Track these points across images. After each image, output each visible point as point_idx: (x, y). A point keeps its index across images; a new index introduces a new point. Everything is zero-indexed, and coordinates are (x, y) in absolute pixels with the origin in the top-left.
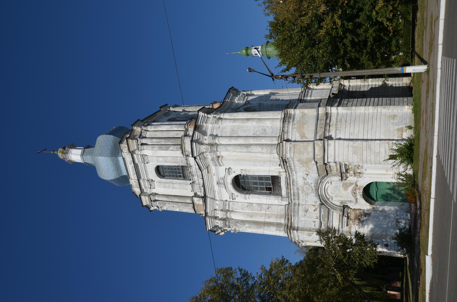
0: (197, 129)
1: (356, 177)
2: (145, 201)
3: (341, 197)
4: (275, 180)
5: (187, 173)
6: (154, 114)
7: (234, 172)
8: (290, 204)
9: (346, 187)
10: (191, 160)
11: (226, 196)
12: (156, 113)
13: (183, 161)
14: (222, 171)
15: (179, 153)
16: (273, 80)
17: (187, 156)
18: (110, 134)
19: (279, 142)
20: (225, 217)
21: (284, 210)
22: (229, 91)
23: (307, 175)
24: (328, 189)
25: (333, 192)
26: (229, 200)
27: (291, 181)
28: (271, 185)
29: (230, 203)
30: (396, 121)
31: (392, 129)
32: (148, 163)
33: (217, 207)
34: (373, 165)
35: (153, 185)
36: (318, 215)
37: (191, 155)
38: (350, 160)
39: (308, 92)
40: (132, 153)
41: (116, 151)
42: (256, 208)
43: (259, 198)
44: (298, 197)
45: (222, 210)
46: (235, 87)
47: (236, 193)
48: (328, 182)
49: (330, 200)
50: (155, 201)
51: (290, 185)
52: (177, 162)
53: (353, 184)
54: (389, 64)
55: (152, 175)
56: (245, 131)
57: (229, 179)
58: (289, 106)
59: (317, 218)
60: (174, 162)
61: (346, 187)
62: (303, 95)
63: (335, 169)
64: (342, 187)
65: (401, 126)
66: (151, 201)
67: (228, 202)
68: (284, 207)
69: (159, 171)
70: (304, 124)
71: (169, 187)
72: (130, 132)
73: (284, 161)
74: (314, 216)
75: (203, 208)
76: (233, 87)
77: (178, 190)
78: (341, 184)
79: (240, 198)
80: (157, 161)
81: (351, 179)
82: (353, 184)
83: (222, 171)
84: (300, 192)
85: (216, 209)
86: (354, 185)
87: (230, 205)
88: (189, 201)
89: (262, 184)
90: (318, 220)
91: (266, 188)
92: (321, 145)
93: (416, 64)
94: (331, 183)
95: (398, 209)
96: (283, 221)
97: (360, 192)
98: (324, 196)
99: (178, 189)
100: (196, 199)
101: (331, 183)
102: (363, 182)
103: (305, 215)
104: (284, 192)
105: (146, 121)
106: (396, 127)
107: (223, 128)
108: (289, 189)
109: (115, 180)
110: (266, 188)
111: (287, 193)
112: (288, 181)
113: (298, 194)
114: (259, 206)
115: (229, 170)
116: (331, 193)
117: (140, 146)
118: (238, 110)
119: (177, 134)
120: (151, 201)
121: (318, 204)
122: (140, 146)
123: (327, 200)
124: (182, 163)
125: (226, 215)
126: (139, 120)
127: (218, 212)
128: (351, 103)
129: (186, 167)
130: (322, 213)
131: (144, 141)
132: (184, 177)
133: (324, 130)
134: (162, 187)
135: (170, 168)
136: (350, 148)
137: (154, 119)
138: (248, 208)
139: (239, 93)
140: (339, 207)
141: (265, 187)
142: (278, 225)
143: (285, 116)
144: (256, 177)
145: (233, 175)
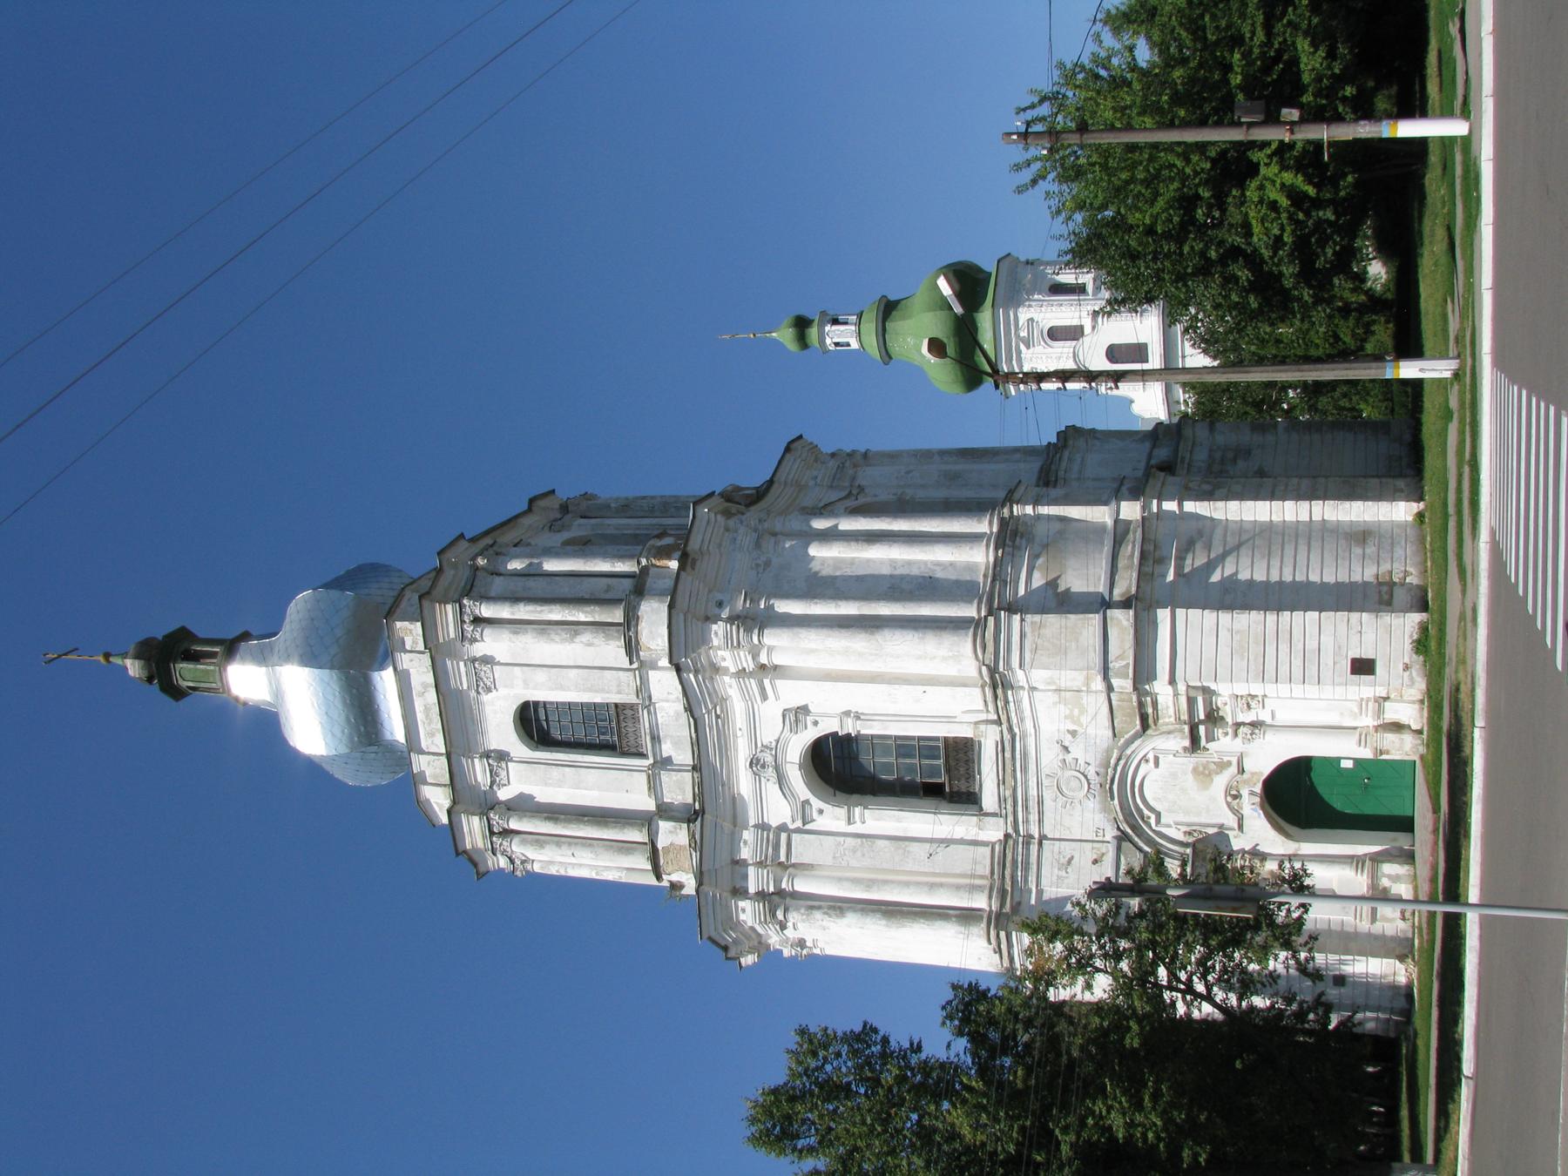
0: (689, 568)
1: (1239, 740)
4: (961, 753)
6: (509, 521)
8: (1011, 842)
9: (1204, 775)
11: (778, 811)
20: (772, 889)
23: (1073, 733)
32: (489, 690)
35: (503, 774)
37: (664, 662)
40: (436, 651)
44: (1041, 813)
47: (816, 803)
48: (1145, 759)
49: (1153, 821)
50: (507, 833)
52: (603, 691)
53: (1229, 763)
55: (499, 729)
57: (797, 745)
58: (1017, 496)
60: (590, 690)
61: (1204, 775)
63: (1171, 712)
66: (492, 833)
68: (988, 850)
69: (535, 724)
73: (998, 683)
76: (800, 437)
79: (831, 816)
80: (526, 683)
81: (1223, 745)
82: (1229, 763)
84: (1048, 796)
86: (1234, 769)
92: (1125, 623)
93: (1326, 674)
94: (1157, 764)
95: (1394, 90)
96: (980, 902)
100: (664, 826)
101: (1157, 764)
102: (1266, 756)
104: (989, 800)
109: (332, 759)
111: (1001, 800)
113: (1040, 802)
117: (469, 628)
119: (609, 588)
121: (1108, 837)
125: (777, 882)
126: (462, 536)
129: (632, 707)
134: (534, 777)
138: (859, 854)
145: (810, 735)
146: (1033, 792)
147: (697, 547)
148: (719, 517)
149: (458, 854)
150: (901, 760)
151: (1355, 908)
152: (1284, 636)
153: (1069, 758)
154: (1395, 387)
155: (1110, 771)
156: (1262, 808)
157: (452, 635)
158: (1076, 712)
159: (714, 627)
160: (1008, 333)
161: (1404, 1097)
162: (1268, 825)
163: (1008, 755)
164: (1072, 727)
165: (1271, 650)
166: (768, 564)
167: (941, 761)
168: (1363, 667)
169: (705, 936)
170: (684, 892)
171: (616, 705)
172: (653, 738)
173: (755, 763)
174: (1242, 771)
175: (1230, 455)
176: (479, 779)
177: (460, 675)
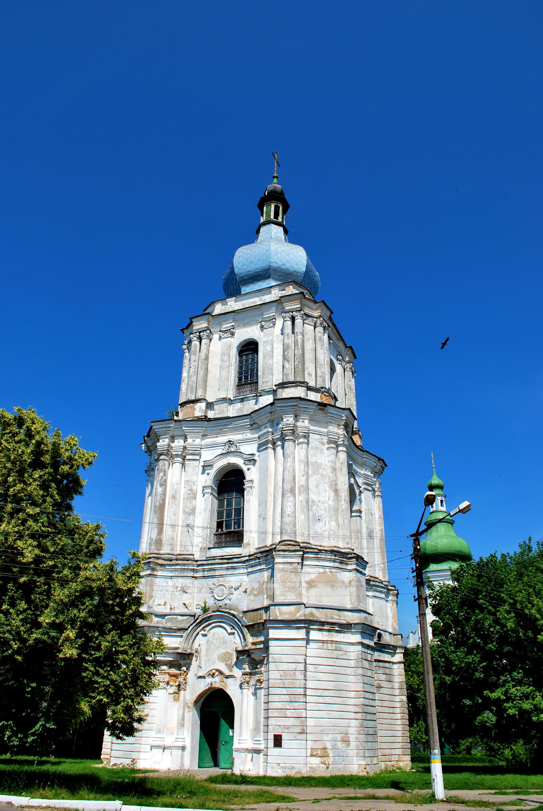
2: (199, 325)
3: (207, 650)
4: (237, 538)
5: (248, 388)
6: (341, 337)
7: (248, 469)
9: (224, 658)
10: (267, 399)
12: (343, 340)
13: (265, 384)
14: (250, 449)
15: (278, 379)
16: (411, 536)
17: (274, 392)
18: (307, 266)
19: (301, 545)
21: (185, 553)
22: (380, 459)
23: (245, 592)
24: (221, 629)
25: (216, 636)
26: (202, 460)
27: (234, 565)
28: (229, 530)
29: (197, 462)
30: (340, 745)
31: (325, 738)
33: (190, 440)
34: (263, 706)
36: (177, 611)
38: (272, 666)
39: (381, 592)
40: (279, 302)
41: (280, 276)
42: (189, 505)
43: (205, 510)
45: (185, 448)
46: (386, 469)
47: (213, 472)
51: (227, 563)
54: (449, 738)
55: (245, 333)
56: (317, 486)
59: (171, 608)
60: (264, 370)
62: (377, 584)
64: (224, 651)
65: (331, 753)
66: (200, 332)
67: (198, 457)
69: (249, 348)
70: (332, 587)
71: (222, 361)
72: (312, 299)
74: (175, 605)
75: (189, 417)
76: (386, 466)
77: (218, 376)
78: (229, 651)
79: (207, 479)
83: (250, 449)
85: (186, 438)
87: (194, 462)
88: (199, 395)
89: (229, 515)
90: (167, 611)
91: (222, 522)
92: (298, 615)
97: (217, 682)
98: (210, 622)
99: (220, 377)
102: (232, 689)
103: (177, 587)
105: (330, 325)
106: (329, 745)
107: (322, 450)
108: (221, 561)
110: (222, 522)
112: (235, 560)
113: (212, 577)
114: (192, 509)
115: (251, 460)
116: (214, 633)
117: (289, 315)
118: (350, 473)
119: (310, 375)
120: (200, 332)
122: (289, 315)
123: (203, 626)
124: (263, 382)
126: (332, 313)
127: (182, 441)
128: (368, 667)
130: (180, 618)
131: (299, 321)
132: (240, 385)
133: (323, 620)
135: (255, 362)
136: (293, 666)
137: (333, 336)
138: (189, 492)
139: (377, 475)
140: (189, 646)
141: (225, 519)
142: (159, 542)
143: (344, 553)
144: (240, 505)
145: (244, 468)
146: (217, 573)
147: (329, 411)
148: (344, 421)
149: (191, 319)
150: (233, 510)
151: (161, 738)
152: (293, 698)
153: (233, 590)
154: (86, 798)
155: (228, 610)
156: (210, 689)
157: (286, 308)
158: (255, 592)
159: (292, 419)
160: (440, 576)
161: (26, 768)
162: (200, 692)
163: (235, 560)
164: (248, 591)
165: (284, 691)
166: (323, 444)
167: (233, 529)
168: (278, 741)
169: (152, 424)
170: (175, 416)
171: (257, 382)
172: (242, 399)
173: (230, 443)
174: (227, 677)
175: (388, 671)
176: (223, 326)
177: (270, 313)
